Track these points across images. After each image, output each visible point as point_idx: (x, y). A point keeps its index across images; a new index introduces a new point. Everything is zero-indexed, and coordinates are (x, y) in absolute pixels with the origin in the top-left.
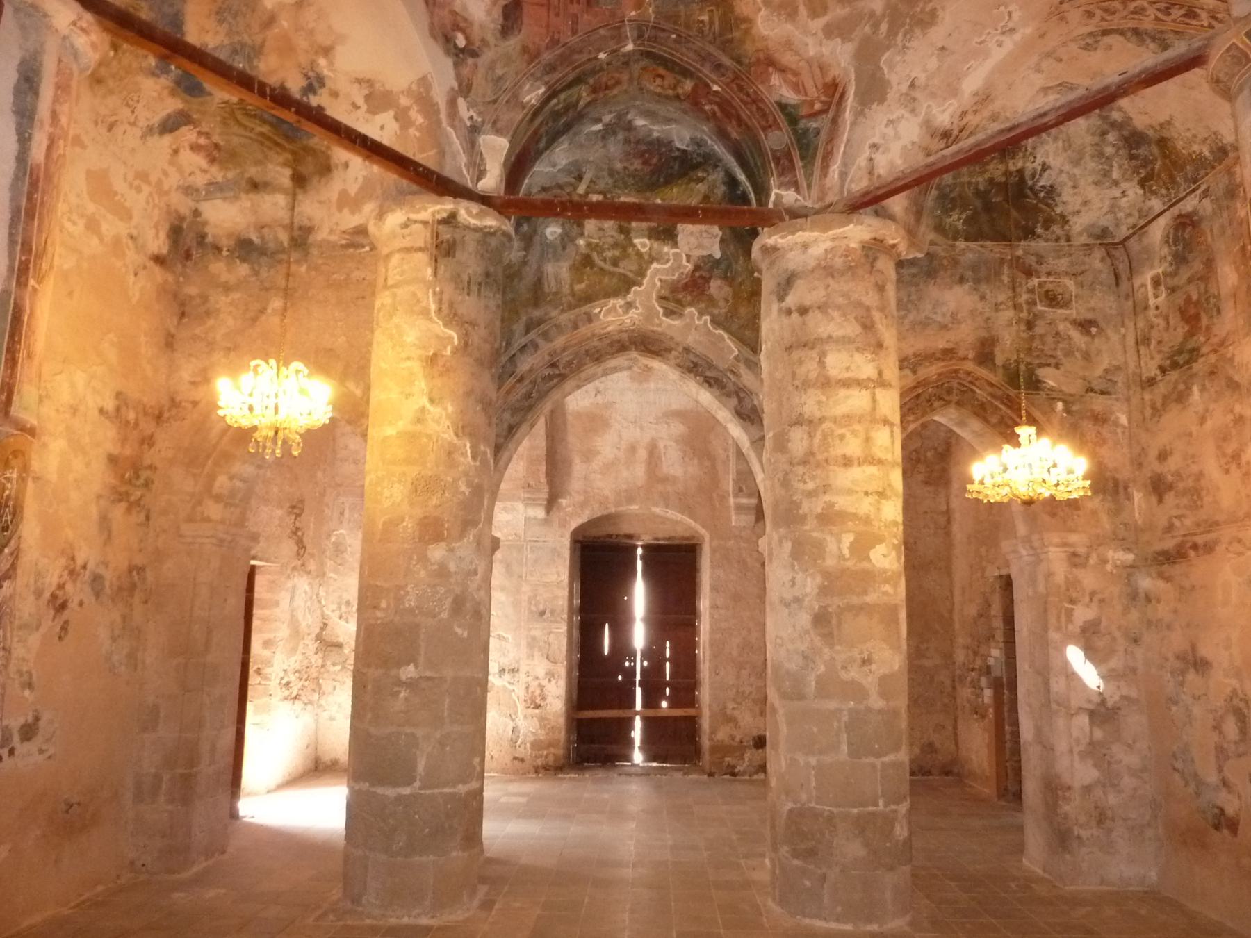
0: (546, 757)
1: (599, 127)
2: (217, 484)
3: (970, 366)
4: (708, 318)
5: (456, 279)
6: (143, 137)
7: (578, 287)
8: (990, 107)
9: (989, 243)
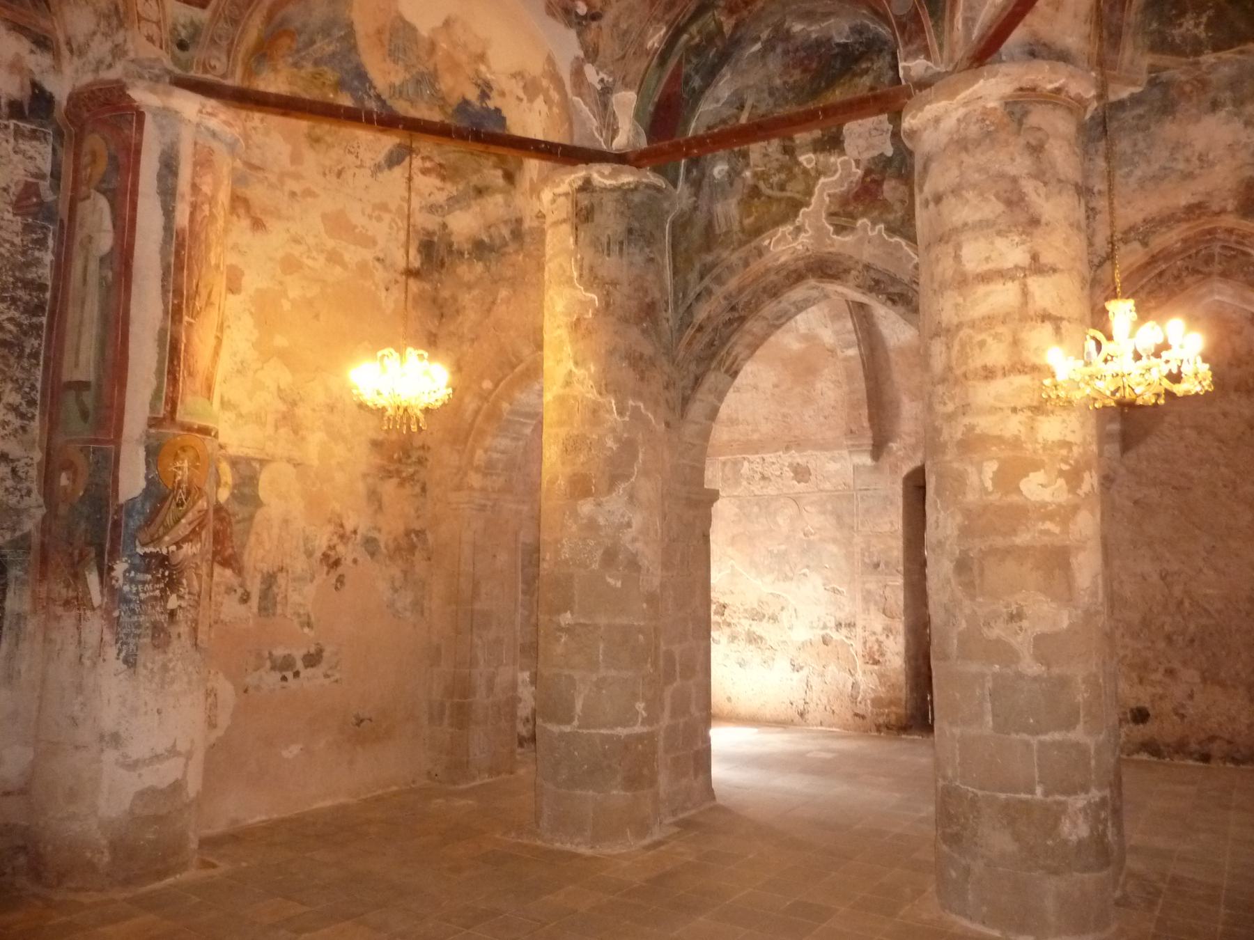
0: (888, 715)
1: (758, 46)
4: (882, 226)
5: (595, 243)
6: (374, 174)
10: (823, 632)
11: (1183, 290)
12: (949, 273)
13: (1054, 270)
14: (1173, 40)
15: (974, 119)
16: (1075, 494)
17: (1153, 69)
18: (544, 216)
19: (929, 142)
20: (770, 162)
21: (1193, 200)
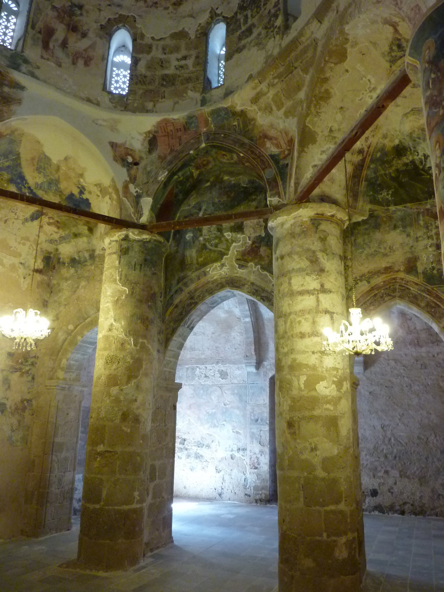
0: (261, 495)
1: (208, 184)
2: (62, 363)
3: (402, 275)
4: (259, 266)
5: (129, 264)
7: (200, 260)
8: (381, 131)
9: (408, 205)
10: (231, 453)
11: (384, 303)
12: (286, 290)
13: (331, 292)
14: (379, 199)
15: (298, 225)
16: (340, 392)
17: (370, 210)
18: (105, 250)
19: (276, 235)
20: (211, 234)
21: (388, 265)
